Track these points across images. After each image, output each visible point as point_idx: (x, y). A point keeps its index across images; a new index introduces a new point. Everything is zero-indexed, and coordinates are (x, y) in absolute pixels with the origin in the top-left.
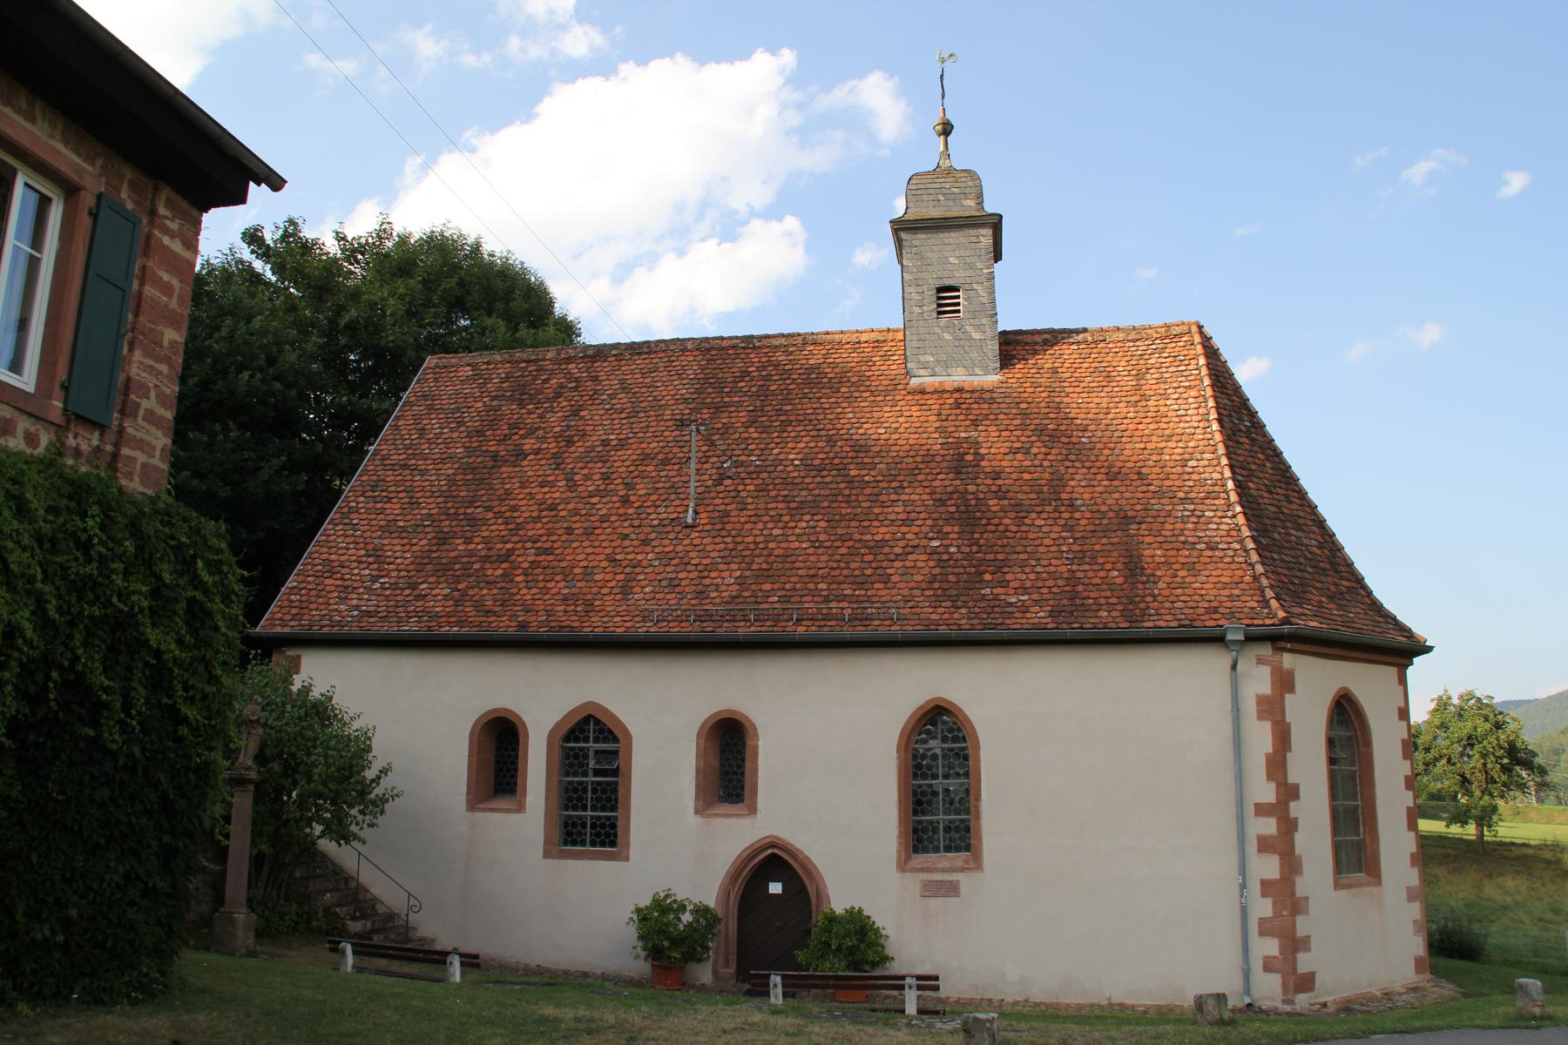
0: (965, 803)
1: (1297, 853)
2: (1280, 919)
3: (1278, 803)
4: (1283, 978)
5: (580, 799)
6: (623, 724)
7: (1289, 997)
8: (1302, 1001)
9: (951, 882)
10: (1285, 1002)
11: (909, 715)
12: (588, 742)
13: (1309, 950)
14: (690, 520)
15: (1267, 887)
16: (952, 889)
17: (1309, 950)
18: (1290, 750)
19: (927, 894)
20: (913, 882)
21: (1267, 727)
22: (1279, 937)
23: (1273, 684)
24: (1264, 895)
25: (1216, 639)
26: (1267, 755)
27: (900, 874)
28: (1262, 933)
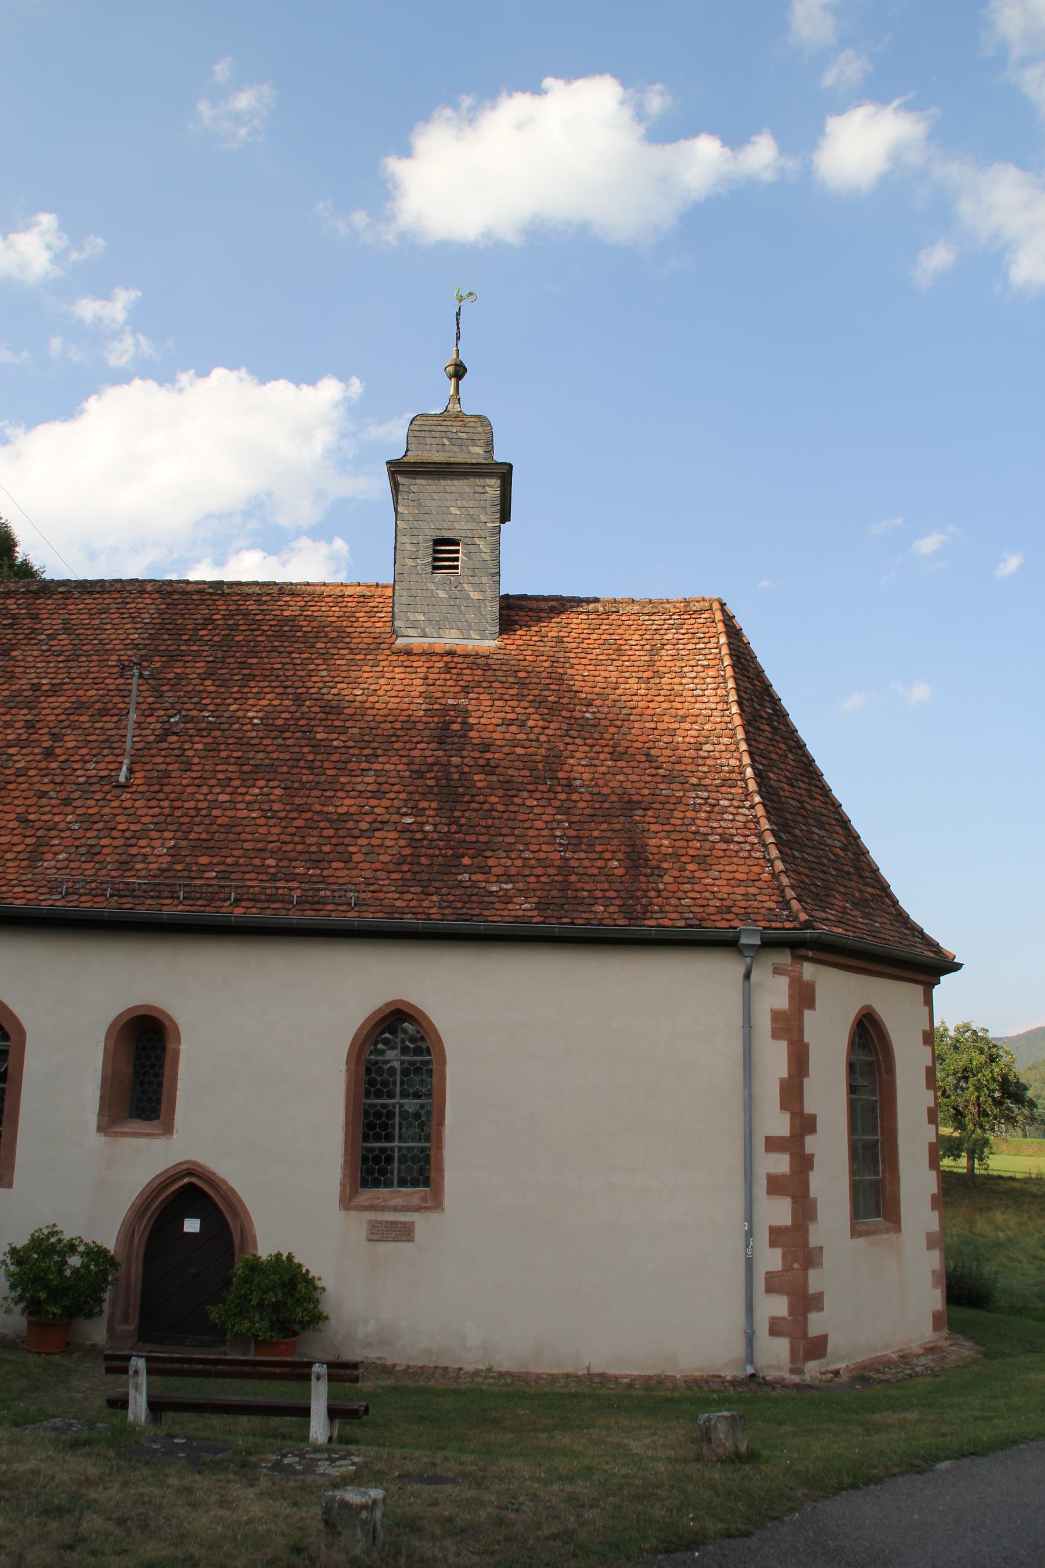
1: (811, 1196)
2: (789, 1274)
3: (792, 1136)
4: (791, 1343)
7: (798, 1365)
9: (404, 1223)
10: (793, 1371)
14: (122, 779)
15: (776, 1235)
19: (376, 1237)
22: (788, 1294)
24: (773, 1244)
25: (728, 943)
27: (343, 1213)
28: (769, 1289)
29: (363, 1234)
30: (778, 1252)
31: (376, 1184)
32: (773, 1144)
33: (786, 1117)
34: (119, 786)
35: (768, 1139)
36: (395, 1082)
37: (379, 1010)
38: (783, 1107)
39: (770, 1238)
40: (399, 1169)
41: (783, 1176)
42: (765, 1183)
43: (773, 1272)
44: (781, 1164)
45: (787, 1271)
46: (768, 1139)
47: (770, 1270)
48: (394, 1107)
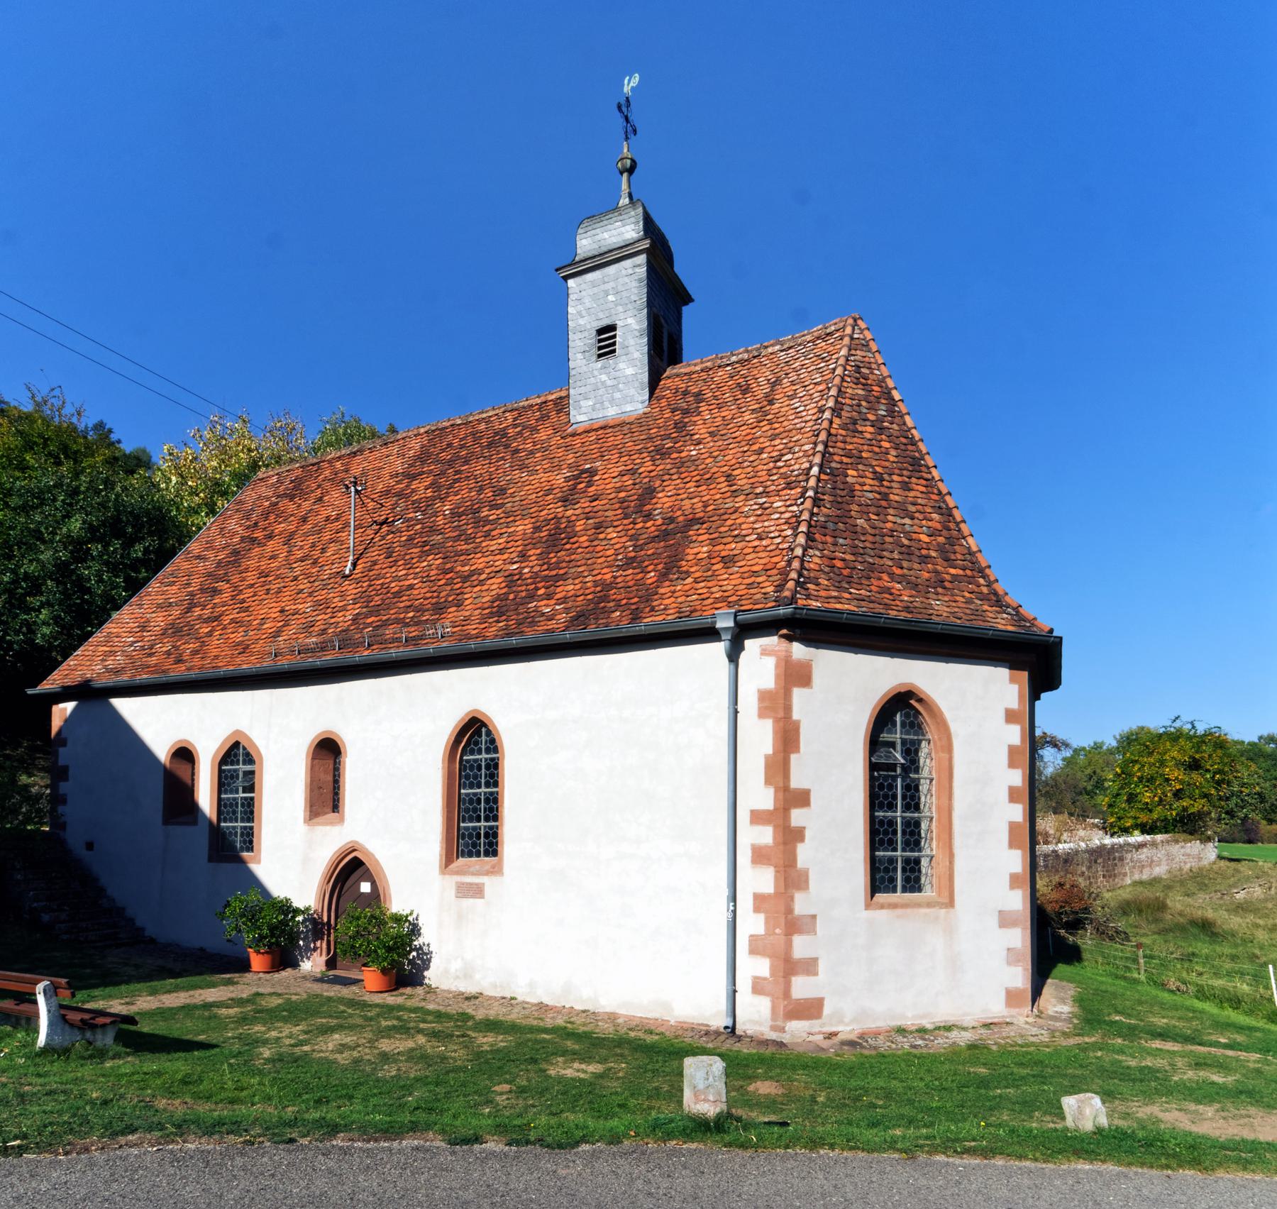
0: (492, 808)
1: (800, 864)
2: (772, 938)
3: (775, 809)
4: (773, 1002)
5: (475, 810)
6: (876, 718)
7: (780, 1023)
8: (798, 1031)
9: (477, 884)
10: (774, 1028)
11: (451, 729)
12: (238, 764)
13: (816, 974)
14: (347, 572)
15: (760, 901)
16: (477, 891)
17: (816, 974)
18: (797, 750)
19: (460, 895)
20: (451, 881)
21: (767, 726)
22: (770, 957)
23: (777, 676)
24: (757, 909)
25: (708, 634)
26: (767, 758)
27: (441, 877)
28: (754, 951)
29: (453, 892)
30: (761, 917)
31: (470, 855)
32: (758, 817)
33: (770, 792)
34: (345, 577)
35: (753, 812)
36: (486, 777)
37: (463, 719)
38: (768, 782)
39: (754, 904)
40: (485, 843)
41: (766, 847)
42: (749, 853)
43: (757, 936)
44: (766, 835)
45: (770, 935)
46: (753, 812)
47: (753, 933)
48: (481, 795)
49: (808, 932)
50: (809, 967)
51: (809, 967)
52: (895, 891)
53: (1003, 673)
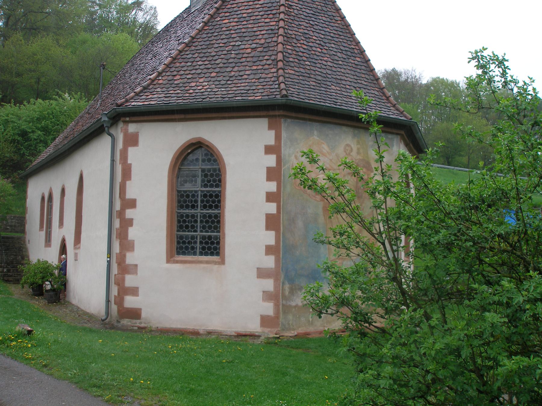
49: (133, 274)
50: (134, 291)
51: (134, 291)
52: (195, 254)
53: (263, 123)
